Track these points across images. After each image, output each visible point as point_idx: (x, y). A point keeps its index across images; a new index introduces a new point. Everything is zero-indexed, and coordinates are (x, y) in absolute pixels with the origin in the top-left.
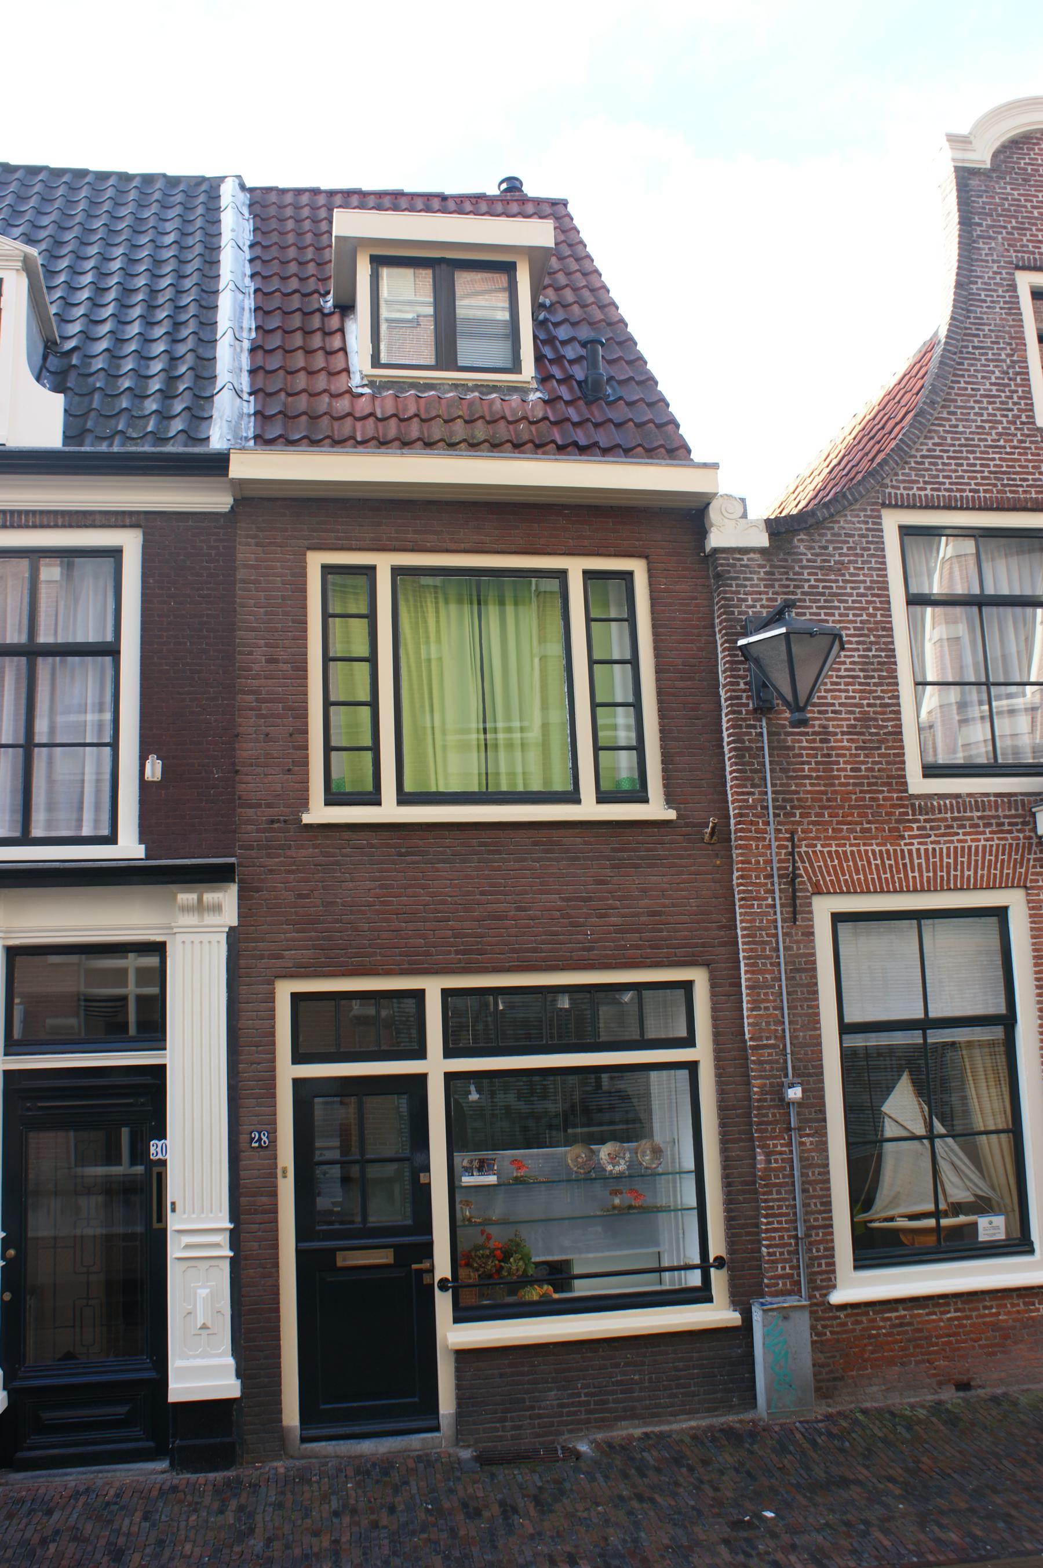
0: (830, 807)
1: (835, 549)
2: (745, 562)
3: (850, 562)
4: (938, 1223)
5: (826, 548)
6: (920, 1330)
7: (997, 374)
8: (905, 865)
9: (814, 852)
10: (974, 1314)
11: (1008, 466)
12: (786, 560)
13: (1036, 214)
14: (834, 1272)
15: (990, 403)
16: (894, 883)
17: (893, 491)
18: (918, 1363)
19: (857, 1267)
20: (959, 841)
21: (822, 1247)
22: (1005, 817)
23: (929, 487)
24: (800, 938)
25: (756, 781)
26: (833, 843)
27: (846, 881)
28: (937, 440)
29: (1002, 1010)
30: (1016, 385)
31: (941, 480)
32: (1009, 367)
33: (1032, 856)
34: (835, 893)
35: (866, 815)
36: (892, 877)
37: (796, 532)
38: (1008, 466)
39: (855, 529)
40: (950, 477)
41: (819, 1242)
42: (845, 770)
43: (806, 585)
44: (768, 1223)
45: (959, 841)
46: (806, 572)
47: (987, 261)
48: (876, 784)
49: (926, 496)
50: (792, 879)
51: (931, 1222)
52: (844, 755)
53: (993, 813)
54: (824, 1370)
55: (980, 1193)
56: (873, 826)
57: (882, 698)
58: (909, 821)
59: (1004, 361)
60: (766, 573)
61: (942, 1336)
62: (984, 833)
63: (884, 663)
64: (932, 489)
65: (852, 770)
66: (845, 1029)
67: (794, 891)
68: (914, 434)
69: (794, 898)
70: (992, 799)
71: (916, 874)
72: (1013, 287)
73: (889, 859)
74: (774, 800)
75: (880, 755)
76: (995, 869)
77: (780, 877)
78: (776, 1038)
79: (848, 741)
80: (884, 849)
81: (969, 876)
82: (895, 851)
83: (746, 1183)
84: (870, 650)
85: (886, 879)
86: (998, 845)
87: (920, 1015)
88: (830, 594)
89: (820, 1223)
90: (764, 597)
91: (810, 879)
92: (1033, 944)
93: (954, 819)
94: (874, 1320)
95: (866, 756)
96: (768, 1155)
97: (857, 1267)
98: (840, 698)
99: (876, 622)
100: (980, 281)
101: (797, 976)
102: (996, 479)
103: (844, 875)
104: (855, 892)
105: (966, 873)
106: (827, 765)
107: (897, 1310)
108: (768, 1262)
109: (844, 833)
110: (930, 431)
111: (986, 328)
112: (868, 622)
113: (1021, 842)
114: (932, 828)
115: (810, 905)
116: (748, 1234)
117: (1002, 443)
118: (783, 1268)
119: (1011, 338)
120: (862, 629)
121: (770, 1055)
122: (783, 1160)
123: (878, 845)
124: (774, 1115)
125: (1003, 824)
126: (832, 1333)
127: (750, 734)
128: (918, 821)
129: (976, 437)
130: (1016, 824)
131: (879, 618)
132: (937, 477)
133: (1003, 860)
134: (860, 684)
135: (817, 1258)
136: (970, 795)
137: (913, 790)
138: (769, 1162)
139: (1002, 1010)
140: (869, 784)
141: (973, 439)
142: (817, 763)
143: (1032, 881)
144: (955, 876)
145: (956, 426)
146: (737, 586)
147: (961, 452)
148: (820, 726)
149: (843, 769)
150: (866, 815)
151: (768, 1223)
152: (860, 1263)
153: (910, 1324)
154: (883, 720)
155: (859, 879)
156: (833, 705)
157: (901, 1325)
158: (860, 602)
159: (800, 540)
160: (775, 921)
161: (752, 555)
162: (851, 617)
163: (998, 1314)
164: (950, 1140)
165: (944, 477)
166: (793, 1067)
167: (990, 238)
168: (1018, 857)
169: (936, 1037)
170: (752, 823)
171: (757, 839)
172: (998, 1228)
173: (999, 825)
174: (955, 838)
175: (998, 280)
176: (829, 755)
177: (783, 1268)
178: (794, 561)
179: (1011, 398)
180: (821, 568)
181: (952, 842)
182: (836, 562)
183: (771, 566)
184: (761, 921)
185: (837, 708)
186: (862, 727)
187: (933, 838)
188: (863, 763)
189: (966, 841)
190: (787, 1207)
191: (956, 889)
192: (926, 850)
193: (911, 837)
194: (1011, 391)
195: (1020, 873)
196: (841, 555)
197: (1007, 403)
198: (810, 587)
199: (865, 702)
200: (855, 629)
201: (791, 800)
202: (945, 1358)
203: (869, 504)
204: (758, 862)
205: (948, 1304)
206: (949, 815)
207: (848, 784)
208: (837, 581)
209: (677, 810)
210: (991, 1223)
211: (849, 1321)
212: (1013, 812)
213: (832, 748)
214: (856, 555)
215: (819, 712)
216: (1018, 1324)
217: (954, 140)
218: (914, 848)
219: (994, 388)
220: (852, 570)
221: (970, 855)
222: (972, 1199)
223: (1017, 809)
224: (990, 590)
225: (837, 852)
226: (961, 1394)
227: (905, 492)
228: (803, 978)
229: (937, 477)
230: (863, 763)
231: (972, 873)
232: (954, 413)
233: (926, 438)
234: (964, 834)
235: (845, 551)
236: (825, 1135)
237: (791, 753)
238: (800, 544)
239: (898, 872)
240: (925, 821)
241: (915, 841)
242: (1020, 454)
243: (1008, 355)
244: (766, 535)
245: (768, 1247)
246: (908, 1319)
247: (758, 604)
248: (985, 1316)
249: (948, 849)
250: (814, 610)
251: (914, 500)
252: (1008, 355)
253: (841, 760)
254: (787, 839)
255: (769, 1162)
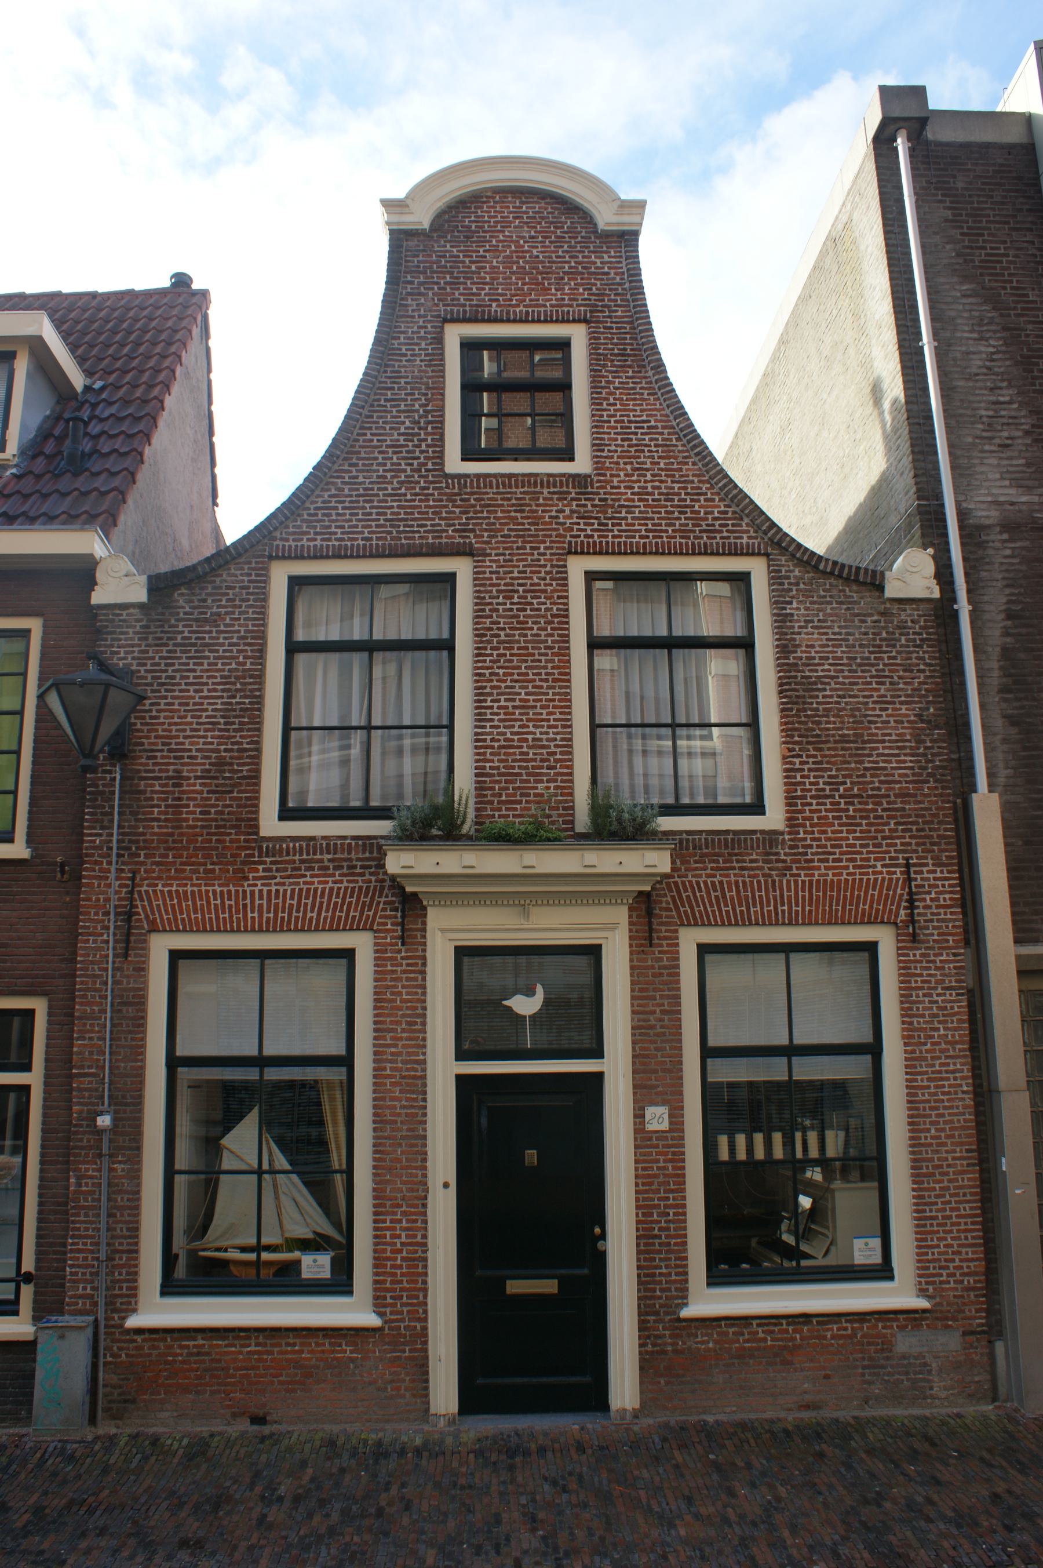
0: (174, 848)
1: (213, 601)
2: (124, 617)
3: (227, 613)
4: (259, 1256)
5: (205, 601)
6: (219, 1361)
7: (408, 424)
8: (245, 906)
9: (155, 892)
10: (276, 1349)
11: (405, 513)
12: (163, 614)
13: (473, 268)
14: (135, 1296)
15: (395, 453)
16: (232, 922)
17: (281, 543)
18: (213, 1392)
19: (709, 1284)
20: (305, 883)
21: (124, 1271)
22: (358, 859)
23: (319, 537)
24: (131, 972)
25: (106, 823)
26: (175, 883)
27: (183, 920)
28: (333, 492)
29: (342, 1051)
30: (426, 434)
31: (333, 530)
32: (420, 417)
33: (383, 899)
34: (171, 931)
35: (210, 856)
36: (231, 917)
37: (176, 587)
38: (405, 513)
39: (237, 582)
40: (343, 527)
41: (122, 1266)
42: (194, 813)
43: (179, 637)
44: (72, 1244)
45: (305, 883)
46: (181, 624)
47: (413, 317)
48: (224, 827)
49: (315, 546)
50: (128, 915)
51: (253, 1256)
52: (195, 799)
53: (346, 855)
54: (116, 1392)
55: (319, 1230)
56: (217, 867)
57: (241, 743)
58: (255, 863)
59: (417, 411)
60: (142, 627)
61: (241, 1369)
62: (333, 875)
63: (247, 709)
64: (322, 540)
65: (201, 813)
66: (708, 1052)
67: (130, 928)
68: (720, 481)
69: (129, 934)
70: (684, 836)
71: (256, 915)
72: (439, 340)
73: (230, 899)
74: (118, 841)
75: (231, 799)
76: (341, 911)
77: (117, 914)
78: (97, 1067)
79: (201, 785)
80: (225, 889)
81: (311, 918)
82: (237, 892)
83: (59, 1204)
84: (234, 697)
85: (224, 919)
86: (346, 888)
87: (254, 1052)
88: (202, 645)
89: (125, 1247)
90: (136, 649)
91: (147, 916)
92: (375, 987)
93: (302, 861)
94: (172, 1347)
95: (217, 799)
96: (79, 1178)
97: (709, 1284)
98: (198, 743)
99: (244, 671)
100: (402, 336)
101: (124, 1009)
102: (392, 526)
103: (182, 913)
104: (192, 931)
105: (309, 915)
106: (177, 809)
107: (195, 1339)
108: (70, 1281)
109: (187, 874)
110: (327, 484)
111: (403, 381)
112: (236, 670)
113: (372, 885)
114: (278, 870)
115: (145, 941)
116: (55, 1253)
117: (403, 491)
118: (85, 1288)
119: (428, 388)
120: (229, 677)
121: (90, 1083)
122: (93, 1184)
123: (220, 885)
124: (89, 1141)
125: (355, 867)
126: (127, 1355)
127: (105, 779)
128: (265, 863)
129: (376, 487)
130: (370, 867)
131: (248, 666)
132: (330, 527)
133: (350, 903)
134: (220, 730)
135: (120, 1281)
136: (324, 838)
137: (264, 832)
138: (79, 1185)
139: (342, 1051)
140: (217, 827)
141: (372, 489)
142: (167, 806)
143: (379, 924)
144: (297, 918)
145: (357, 477)
146: (113, 639)
147: (358, 502)
148: (175, 771)
149: (192, 813)
150: (210, 856)
151: (72, 1244)
152: (712, 1280)
153: (208, 1354)
154: (238, 765)
155: (196, 918)
156: (190, 750)
157: (198, 1354)
158: (231, 651)
159: (182, 594)
160: (107, 956)
161: (131, 611)
162: (220, 666)
163: (301, 1352)
164: (294, 1177)
165: (337, 527)
166: (110, 1097)
167: (420, 294)
168: (368, 900)
169: (273, 1074)
170: (96, 863)
171: (100, 878)
172: (323, 1266)
173: (349, 867)
174: (302, 880)
175: (422, 334)
176: (180, 799)
177: (85, 1288)
178: (171, 614)
179: (420, 446)
180: (197, 620)
181: (298, 883)
182: (212, 614)
183: (149, 620)
184: (95, 956)
185: (194, 753)
186: (217, 771)
187: (278, 880)
188: (213, 806)
189: (313, 883)
190: (94, 1229)
191: (296, 930)
192: (269, 892)
193: (255, 878)
194: (419, 440)
195: (368, 916)
196: (218, 607)
197: (414, 452)
198: (183, 638)
199: (222, 747)
200: (222, 677)
201: (137, 842)
202: (242, 1391)
203: (254, 557)
204: (98, 900)
205: (249, 1338)
206: (297, 857)
207: (196, 827)
208: (210, 632)
209: (34, 850)
210: (315, 1261)
211: (146, 1345)
212: (367, 855)
213: (183, 792)
214: (235, 606)
215: (175, 758)
216: (322, 1364)
217: (388, 204)
218: (256, 889)
219: (402, 438)
220: (228, 621)
221: (315, 897)
222: (311, 1236)
223: (371, 852)
224: (677, 632)
225: (177, 891)
226: (256, 1427)
227: (293, 544)
228: (131, 1011)
229: (330, 527)
230: (213, 806)
231: (315, 915)
232: (356, 465)
233: (323, 490)
234: (312, 876)
235: (224, 603)
236: (139, 1162)
237: (142, 797)
238: (181, 599)
239: (237, 912)
240: (272, 863)
241: (259, 883)
242: (420, 501)
243: (421, 406)
244: (145, 591)
245: (72, 1266)
246: (206, 1349)
247: (130, 657)
248: (286, 1352)
249: (293, 890)
250: (184, 660)
251: (302, 551)
252: (421, 406)
253: (192, 803)
254: (128, 879)
255: (79, 1185)
